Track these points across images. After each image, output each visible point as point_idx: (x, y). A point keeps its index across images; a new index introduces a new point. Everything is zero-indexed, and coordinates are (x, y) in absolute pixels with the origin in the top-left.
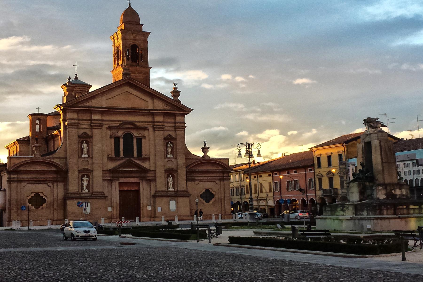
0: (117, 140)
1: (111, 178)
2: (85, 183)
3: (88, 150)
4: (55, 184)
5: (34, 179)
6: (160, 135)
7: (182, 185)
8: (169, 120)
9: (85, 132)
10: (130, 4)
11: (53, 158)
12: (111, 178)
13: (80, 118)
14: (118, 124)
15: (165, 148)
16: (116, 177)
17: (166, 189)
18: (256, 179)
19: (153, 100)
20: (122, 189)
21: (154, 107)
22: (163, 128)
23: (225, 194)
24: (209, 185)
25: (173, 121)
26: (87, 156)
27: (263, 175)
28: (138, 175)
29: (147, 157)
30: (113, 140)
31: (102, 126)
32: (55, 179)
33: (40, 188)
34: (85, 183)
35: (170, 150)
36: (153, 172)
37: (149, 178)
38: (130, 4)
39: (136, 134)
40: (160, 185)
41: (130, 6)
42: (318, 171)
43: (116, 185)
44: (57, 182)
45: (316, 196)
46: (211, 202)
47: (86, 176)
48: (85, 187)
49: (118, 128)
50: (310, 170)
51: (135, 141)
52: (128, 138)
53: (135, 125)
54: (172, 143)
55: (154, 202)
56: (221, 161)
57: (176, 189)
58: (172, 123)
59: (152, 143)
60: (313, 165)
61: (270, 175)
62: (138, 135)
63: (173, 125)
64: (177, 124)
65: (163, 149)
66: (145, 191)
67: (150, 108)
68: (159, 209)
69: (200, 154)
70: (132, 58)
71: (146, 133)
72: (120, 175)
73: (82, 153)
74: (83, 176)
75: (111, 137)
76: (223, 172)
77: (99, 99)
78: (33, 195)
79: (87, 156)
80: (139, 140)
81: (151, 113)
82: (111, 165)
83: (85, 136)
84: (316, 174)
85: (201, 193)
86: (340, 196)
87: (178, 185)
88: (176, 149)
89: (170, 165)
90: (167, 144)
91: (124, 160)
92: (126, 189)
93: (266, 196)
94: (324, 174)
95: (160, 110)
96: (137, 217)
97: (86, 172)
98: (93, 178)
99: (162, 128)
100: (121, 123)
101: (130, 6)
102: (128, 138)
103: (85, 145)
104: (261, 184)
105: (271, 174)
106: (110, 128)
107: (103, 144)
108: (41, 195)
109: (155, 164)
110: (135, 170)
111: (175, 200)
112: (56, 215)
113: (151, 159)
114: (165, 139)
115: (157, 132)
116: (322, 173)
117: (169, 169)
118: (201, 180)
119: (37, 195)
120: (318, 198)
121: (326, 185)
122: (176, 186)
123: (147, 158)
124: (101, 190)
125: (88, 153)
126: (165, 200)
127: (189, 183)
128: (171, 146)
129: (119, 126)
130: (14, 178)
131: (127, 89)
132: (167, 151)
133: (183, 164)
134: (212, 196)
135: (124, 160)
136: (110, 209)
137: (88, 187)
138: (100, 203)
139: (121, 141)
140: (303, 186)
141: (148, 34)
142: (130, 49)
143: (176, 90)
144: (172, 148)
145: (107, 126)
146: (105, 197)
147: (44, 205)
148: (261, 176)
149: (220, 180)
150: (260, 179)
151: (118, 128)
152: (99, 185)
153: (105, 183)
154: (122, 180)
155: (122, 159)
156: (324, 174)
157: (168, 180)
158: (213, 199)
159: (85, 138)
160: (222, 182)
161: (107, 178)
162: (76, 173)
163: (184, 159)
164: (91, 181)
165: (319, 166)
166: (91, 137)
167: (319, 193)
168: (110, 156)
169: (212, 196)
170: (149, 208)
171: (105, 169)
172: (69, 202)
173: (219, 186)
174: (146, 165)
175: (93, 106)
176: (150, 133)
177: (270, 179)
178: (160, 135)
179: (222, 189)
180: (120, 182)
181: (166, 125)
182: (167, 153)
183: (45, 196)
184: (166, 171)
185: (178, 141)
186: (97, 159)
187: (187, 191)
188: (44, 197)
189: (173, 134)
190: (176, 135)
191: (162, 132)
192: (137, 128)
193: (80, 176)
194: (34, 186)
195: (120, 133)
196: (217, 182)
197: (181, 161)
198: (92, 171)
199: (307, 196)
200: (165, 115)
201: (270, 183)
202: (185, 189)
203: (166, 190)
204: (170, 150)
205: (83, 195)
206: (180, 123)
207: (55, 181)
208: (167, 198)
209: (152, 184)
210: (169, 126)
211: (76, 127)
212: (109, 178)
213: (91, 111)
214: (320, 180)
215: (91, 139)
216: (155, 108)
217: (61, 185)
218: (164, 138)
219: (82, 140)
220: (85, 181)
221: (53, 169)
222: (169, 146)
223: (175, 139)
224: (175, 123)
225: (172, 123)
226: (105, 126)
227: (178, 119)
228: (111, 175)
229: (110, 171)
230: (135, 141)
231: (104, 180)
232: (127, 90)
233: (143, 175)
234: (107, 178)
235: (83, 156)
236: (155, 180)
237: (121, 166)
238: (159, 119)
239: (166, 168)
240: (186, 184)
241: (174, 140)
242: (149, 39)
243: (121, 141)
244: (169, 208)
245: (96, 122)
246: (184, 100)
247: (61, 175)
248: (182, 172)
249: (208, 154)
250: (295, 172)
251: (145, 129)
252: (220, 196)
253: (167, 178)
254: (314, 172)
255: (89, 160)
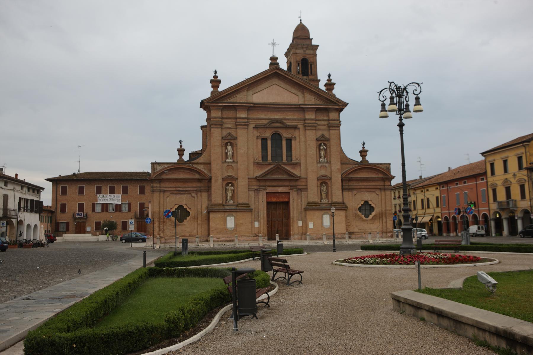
0: (264, 141)
1: (258, 187)
2: (230, 194)
3: (233, 153)
4: (199, 195)
5: (177, 189)
6: (312, 135)
7: (337, 195)
8: (322, 118)
9: (229, 133)
10: (301, 20)
11: (197, 163)
12: (258, 187)
13: (225, 116)
14: (264, 122)
15: (318, 150)
16: (263, 186)
17: (319, 200)
18: (423, 193)
19: (303, 94)
20: (270, 200)
21: (304, 101)
22: (315, 127)
23: (386, 207)
24: (367, 196)
25: (326, 118)
26: (231, 161)
27: (430, 189)
28: (287, 183)
29: (297, 161)
30: (260, 142)
31: (248, 125)
32: (199, 189)
33: (184, 200)
34: (230, 194)
35: (323, 153)
36: (304, 180)
37: (300, 187)
38: (301, 20)
39: (285, 135)
40: (313, 194)
41: (301, 22)
42: (491, 179)
43: (262, 197)
44: (201, 191)
45: (489, 210)
46: (371, 217)
47: (230, 185)
48: (229, 198)
49: (265, 127)
50: (482, 179)
51: (284, 143)
52: (277, 138)
53: (283, 123)
54: (325, 145)
55: (306, 216)
56: (380, 166)
57: (330, 200)
58: (325, 120)
59: (304, 146)
60: (485, 174)
61: (437, 188)
62: (288, 136)
63: (326, 123)
64: (330, 122)
65: (315, 152)
66: (296, 204)
67: (301, 102)
68: (311, 225)
69: (359, 159)
70: (302, 73)
71: (296, 133)
72: (268, 183)
73: (227, 157)
74: (227, 184)
75: (258, 138)
76: (383, 180)
77: (245, 93)
78: (176, 207)
79: (231, 161)
80: (289, 141)
81: (301, 108)
82: (259, 173)
83: (229, 137)
84: (489, 184)
85: (359, 206)
86: (520, 210)
87: (332, 195)
88: (330, 151)
89: (323, 172)
90: (320, 145)
91: (272, 166)
92: (274, 200)
93: (433, 211)
94: (499, 183)
95: (311, 105)
96: (277, 235)
97: (230, 181)
98: (237, 187)
99: (314, 127)
100: (268, 121)
101: (301, 22)
102: (277, 138)
103: (229, 148)
104: (428, 200)
105: (438, 187)
106: (256, 127)
107: (248, 145)
108: (185, 207)
109: (306, 169)
110: (284, 177)
111: (233, 216)
112: (200, 232)
113: (302, 165)
114: (317, 140)
115: (308, 132)
116: (497, 182)
117: (324, 176)
118: (359, 190)
119: (181, 207)
120: (492, 212)
121: (502, 196)
122: (330, 197)
123: (297, 163)
124: (245, 201)
125: (233, 157)
126: (317, 213)
127: (346, 193)
128: (324, 148)
129: (266, 124)
130: (156, 187)
131: (275, 81)
132: (320, 154)
133: (338, 169)
134: (372, 209)
135: (272, 166)
136: (256, 224)
137: (232, 197)
138: (245, 217)
139: (269, 142)
140: (275, 278)
141: (317, 47)
142: (300, 63)
143: (330, 82)
144: (326, 150)
145: (254, 125)
146: (251, 211)
147: (188, 218)
148: (428, 190)
149: (380, 189)
150: (427, 193)
151: (265, 127)
152: (243, 194)
153: (251, 193)
154: (270, 190)
155: (270, 164)
156: (499, 183)
157: (322, 189)
158: (373, 214)
159: (229, 140)
160: (383, 193)
161: (253, 187)
162: (220, 181)
163: (339, 164)
164: (235, 190)
165: (493, 173)
166: (236, 138)
167: (494, 207)
168: (257, 161)
169: (372, 209)
170: (300, 223)
171: (251, 176)
172: (212, 215)
173: (380, 197)
174: (296, 172)
175: (238, 101)
176: (301, 133)
177: (437, 193)
178: (312, 135)
179: (383, 201)
180: (268, 191)
181: (319, 122)
182: (320, 157)
183: (189, 208)
184: (318, 179)
185: (333, 142)
186: (242, 164)
187: (343, 203)
188: (188, 209)
189: (326, 134)
190: (330, 135)
191: (314, 131)
192: (287, 127)
193: (224, 184)
194: (178, 197)
195: (268, 134)
196: (378, 192)
197: (336, 166)
198: (237, 178)
199: (479, 210)
200: (318, 110)
201: (437, 198)
202: (341, 200)
203: (320, 202)
204: (323, 153)
205: (227, 207)
206: (334, 120)
207: (198, 191)
208: (320, 211)
209: (303, 193)
210: (322, 125)
211: (218, 126)
212: (256, 187)
213: (234, 108)
214: (494, 191)
215: (235, 141)
216: (306, 103)
217: (205, 195)
218: (316, 139)
219: (226, 141)
220: (230, 191)
221: (197, 176)
222: (322, 148)
223: (329, 140)
224: (329, 120)
225: (325, 120)
226: (251, 126)
227: (333, 115)
228: (258, 184)
229: (258, 179)
230: (284, 143)
231: (249, 190)
232: (275, 83)
233: (293, 183)
234: (253, 187)
235: (228, 160)
236: (306, 189)
237: (267, 173)
238: (310, 116)
239: (318, 176)
240: (341, 195)
241: (327, 142)
242: (318, 52)
243: (269, 142)
244: (322, 223)
245: (241, 120)
246: (338, 92)
247: (205, 182)
248: (337, 179)
249: (367, 158)
250: (465, 183)
251: (296, 128)
252: (380, 209)
253: (321, 187)
254: (487, 182)
255: (233, 165)
